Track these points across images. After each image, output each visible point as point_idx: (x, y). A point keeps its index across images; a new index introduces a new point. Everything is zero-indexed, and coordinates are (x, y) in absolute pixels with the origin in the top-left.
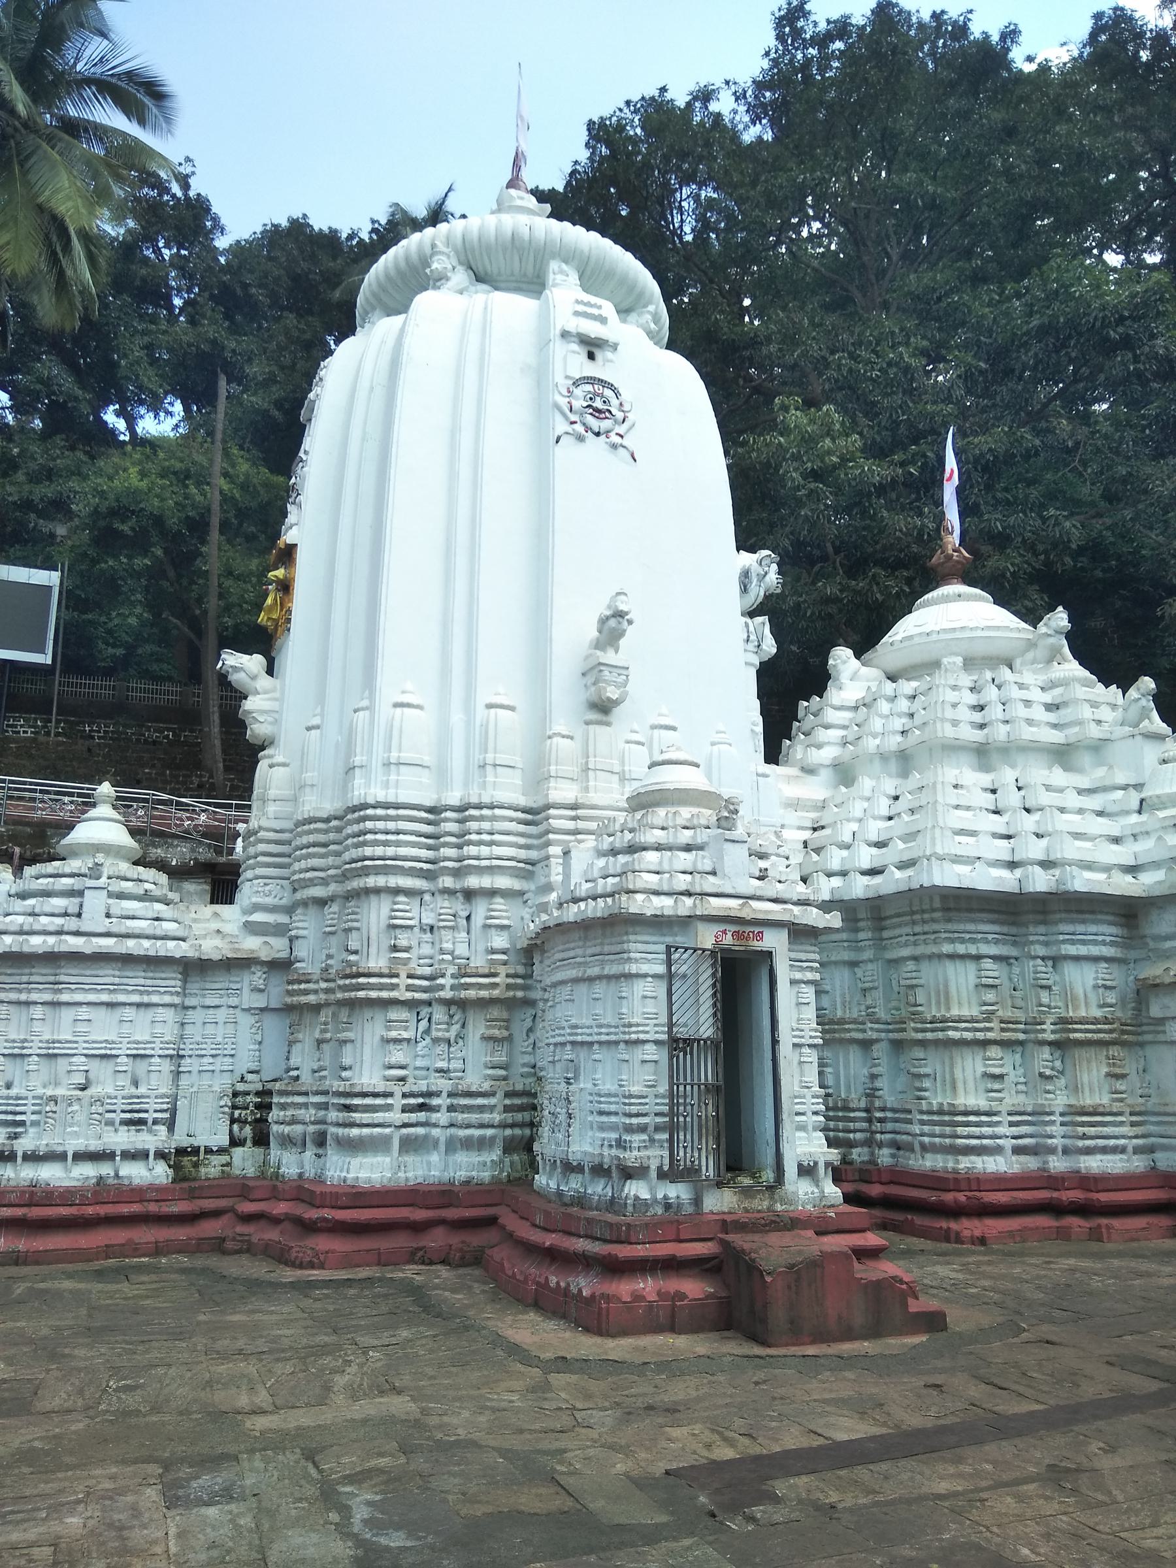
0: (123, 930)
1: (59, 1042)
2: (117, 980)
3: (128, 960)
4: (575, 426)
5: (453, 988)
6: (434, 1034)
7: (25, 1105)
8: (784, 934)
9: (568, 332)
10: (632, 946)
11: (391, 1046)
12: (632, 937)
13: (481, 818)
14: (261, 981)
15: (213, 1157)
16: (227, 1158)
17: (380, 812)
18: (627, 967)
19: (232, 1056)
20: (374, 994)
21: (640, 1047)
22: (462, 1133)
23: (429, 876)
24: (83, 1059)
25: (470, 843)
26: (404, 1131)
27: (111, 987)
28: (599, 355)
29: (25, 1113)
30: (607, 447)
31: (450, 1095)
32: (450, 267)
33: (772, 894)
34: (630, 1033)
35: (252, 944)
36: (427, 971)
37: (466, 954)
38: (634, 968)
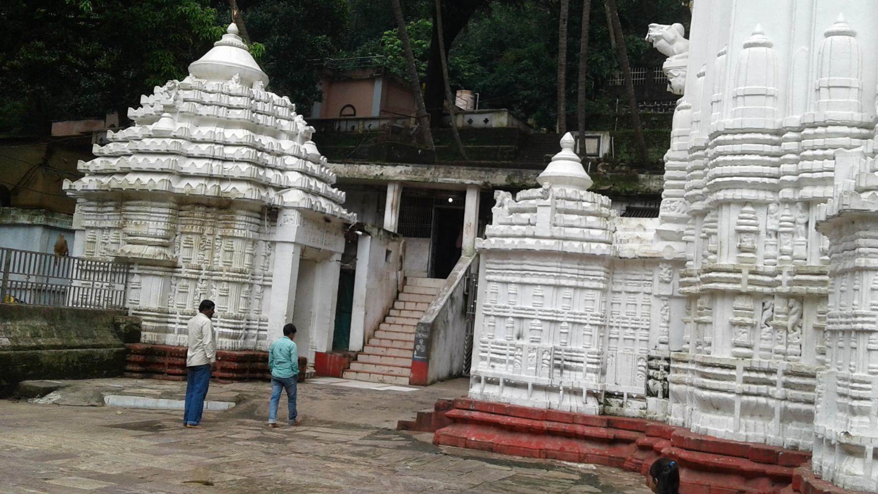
0: (562, 235)
1: (524, 309)
2: (559, 270)
3: (566, 256)
6: (775, 322)
7: (506, 349)
10: (861, 241)
11: (737, 329)
12: (862, 233)
13: (816, 136)
14: (667, 275)
15: (634, 402)
16: (644, 403)
17: (729, 137)
18: (857, 261)
19: (648, 330)
20: (722, 286)
21: (867, 336)
22: (792, 406)
23: (775, 189)
24: (539, 322)
25: (804, 158)
26: (745, 398)
27: (555, 274)
29: (505, 355)
31: (786, 374)
34: (856, 323)
35: (659, 248)
38: (862, 262)
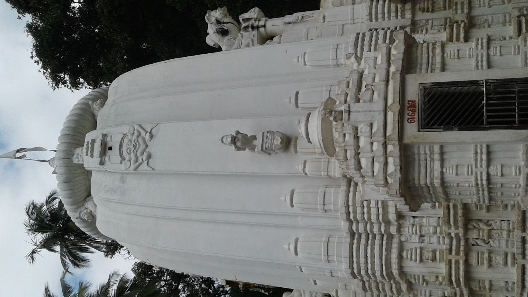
4: (144, 159)
5: (457, 228)
8: (410, 78)
9: (100, 162)
10: (422, 182)
12: (416, 182)
13: (355, 212)
17: (355, 266)
20: (462, 273)
21: (492, 177)
23: (391, 237)
28: (109, 145)
30: (152, 141)
32: (85, 211)
33: (382, 85)
34: (482, 185)
36: (447, 240)
37: (435, 219)
38: (437, 182)
